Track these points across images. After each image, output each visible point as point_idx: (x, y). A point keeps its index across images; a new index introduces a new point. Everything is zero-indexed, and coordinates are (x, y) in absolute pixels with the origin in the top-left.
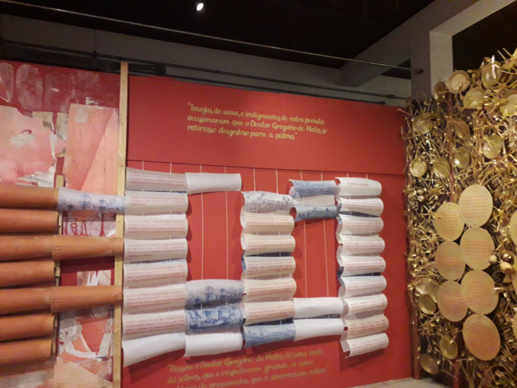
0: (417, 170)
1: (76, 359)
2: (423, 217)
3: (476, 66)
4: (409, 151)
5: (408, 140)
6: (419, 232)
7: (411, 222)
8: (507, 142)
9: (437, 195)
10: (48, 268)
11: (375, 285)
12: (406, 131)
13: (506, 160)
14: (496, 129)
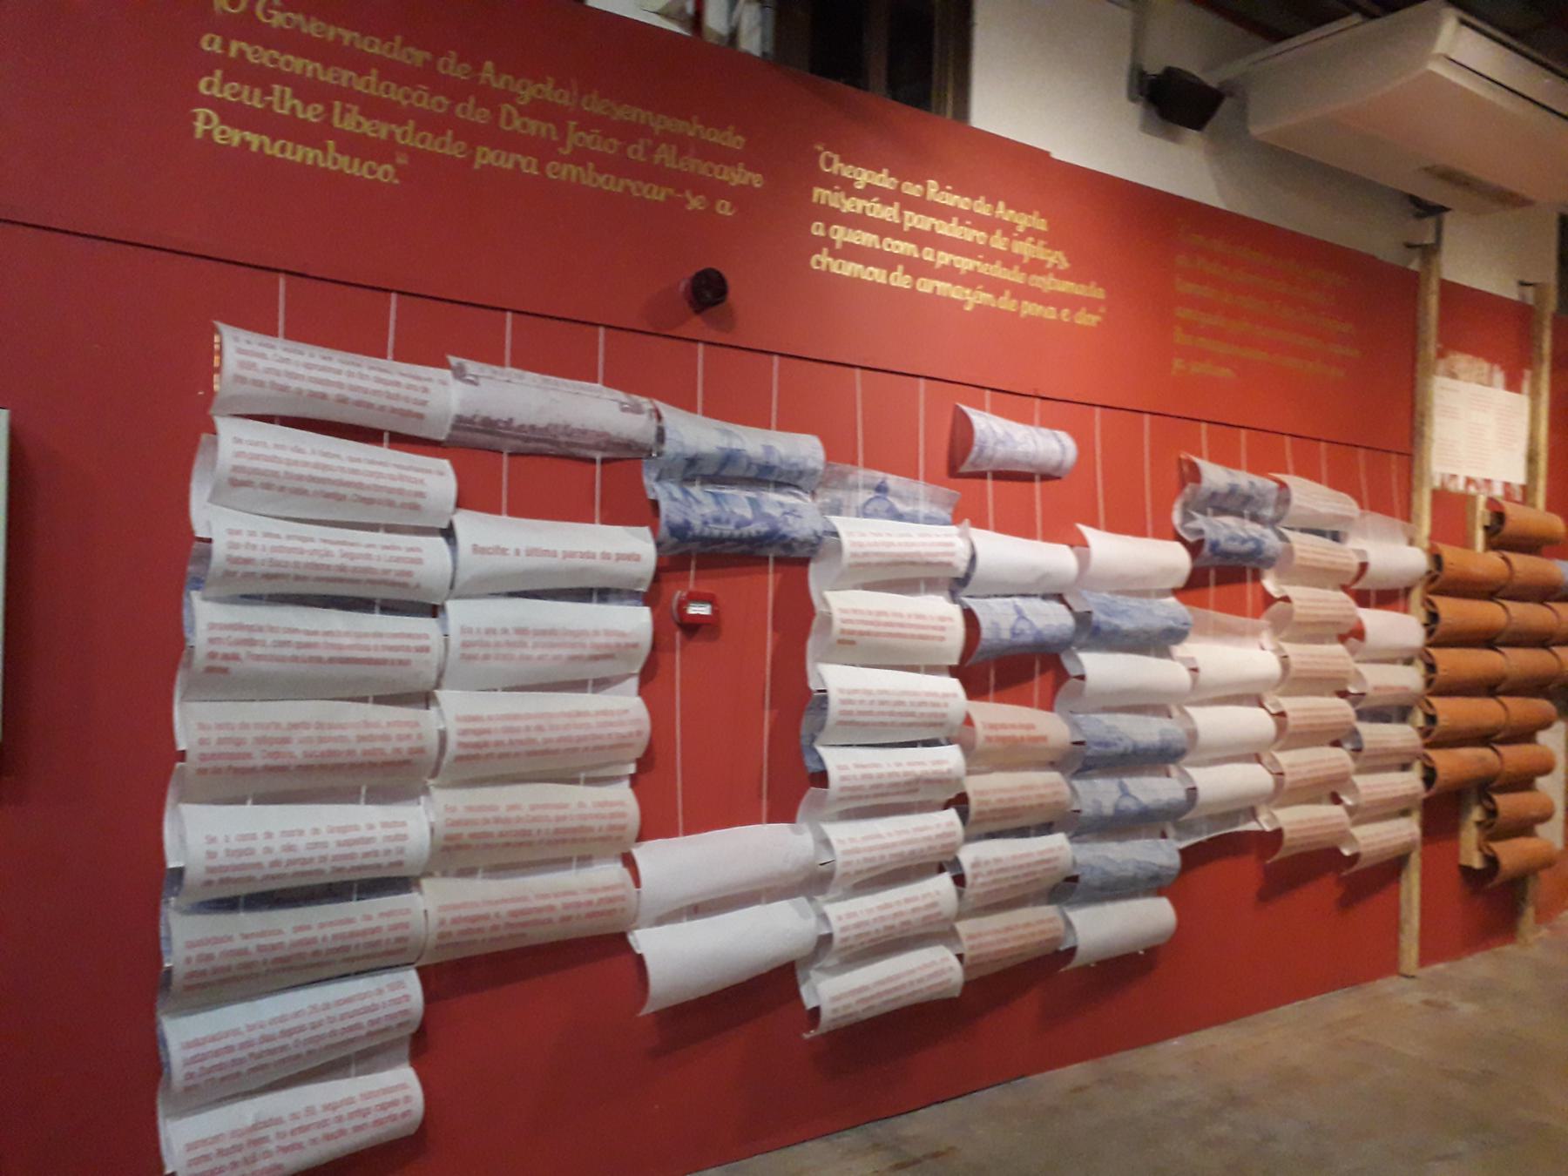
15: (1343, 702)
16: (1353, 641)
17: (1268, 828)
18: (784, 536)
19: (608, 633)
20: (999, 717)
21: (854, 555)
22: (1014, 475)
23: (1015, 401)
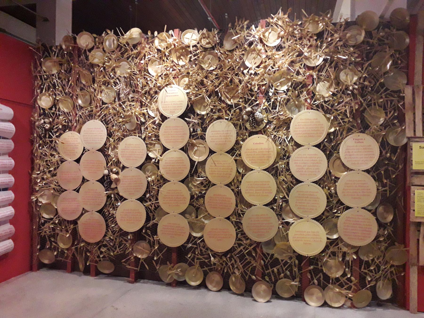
0: (45, 102)
2: (48, 141)
3: (100, 34)
4: (37, 85)
5: (37, 76)
6: (44, 153)
7: (37, 145)
8: (119, 94)
9: (61, 124)
11: (5, 198)
12: (36, 68)
13: (118, 105)
14: (111, 83)
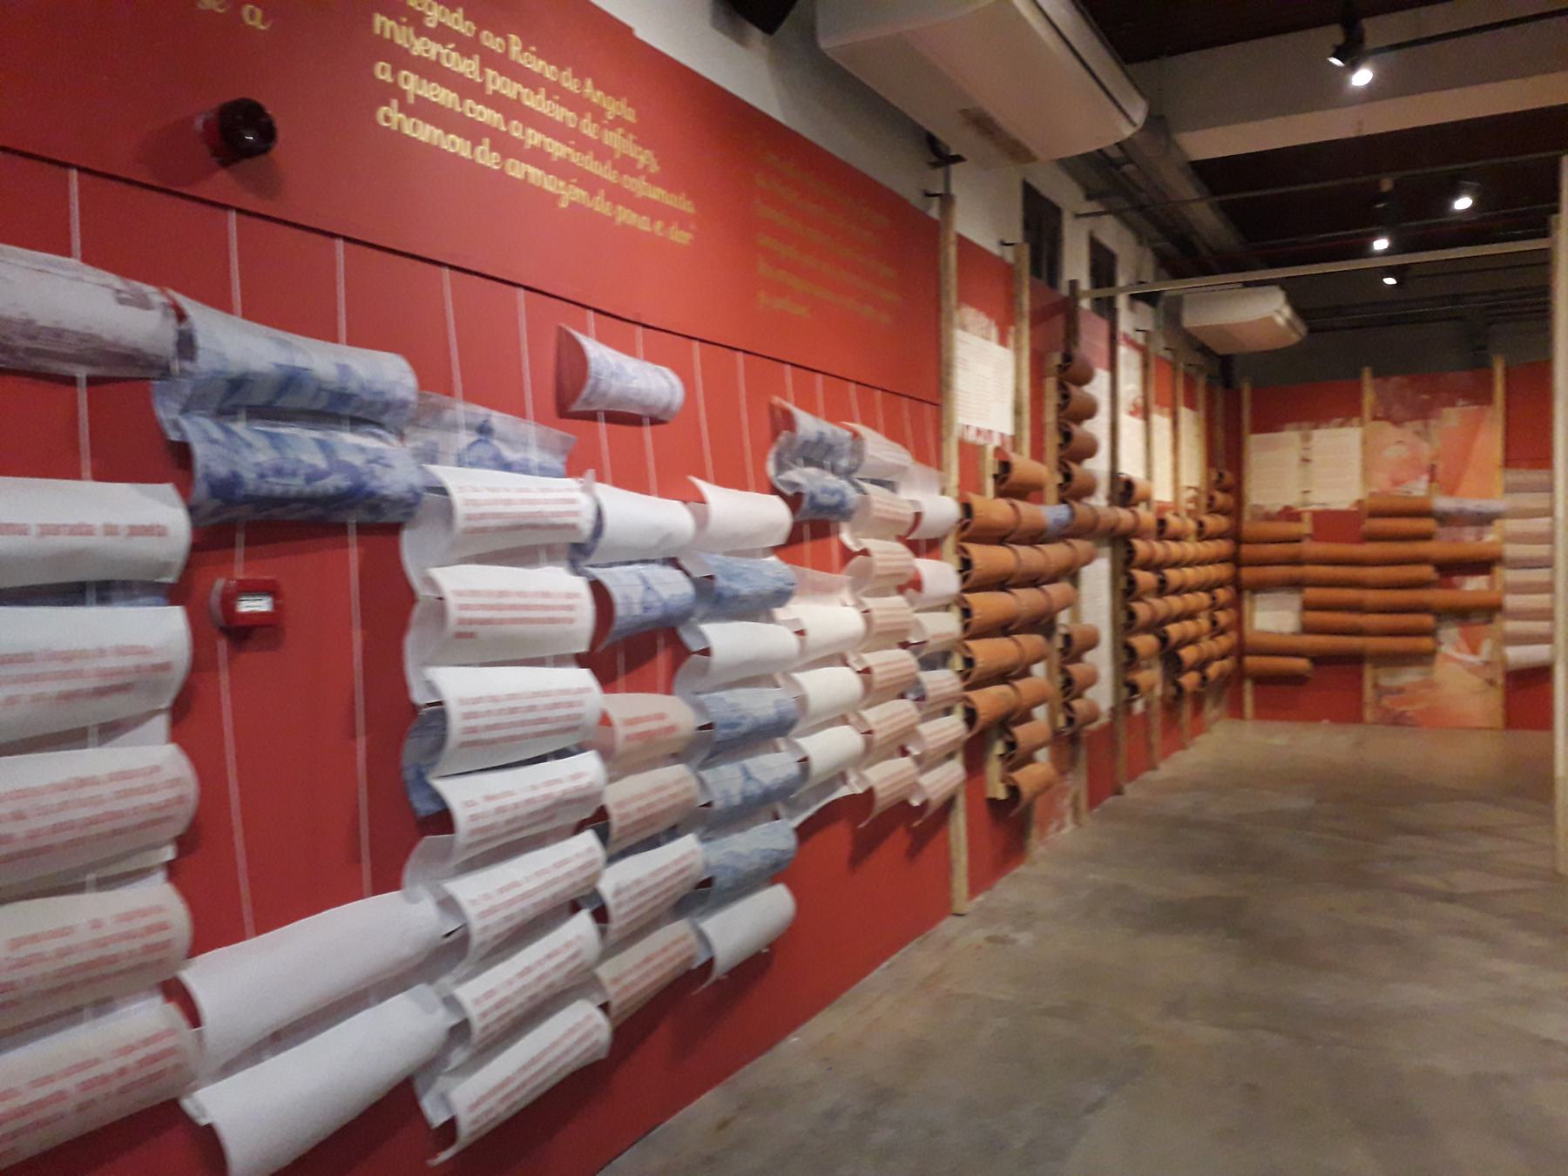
1: (1455, 660)
10: (1427, 572)
15: (904, 654)
16: (910, 591)
17: (859, 791)
18: (371, 494)
19: (121, 651)
20: (640, 710)
21: (469, 517)
22: (625, 418)
23: (621, 326)
